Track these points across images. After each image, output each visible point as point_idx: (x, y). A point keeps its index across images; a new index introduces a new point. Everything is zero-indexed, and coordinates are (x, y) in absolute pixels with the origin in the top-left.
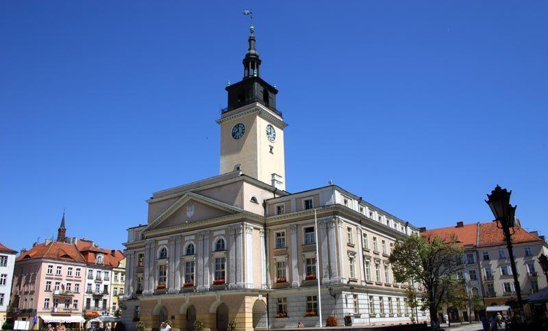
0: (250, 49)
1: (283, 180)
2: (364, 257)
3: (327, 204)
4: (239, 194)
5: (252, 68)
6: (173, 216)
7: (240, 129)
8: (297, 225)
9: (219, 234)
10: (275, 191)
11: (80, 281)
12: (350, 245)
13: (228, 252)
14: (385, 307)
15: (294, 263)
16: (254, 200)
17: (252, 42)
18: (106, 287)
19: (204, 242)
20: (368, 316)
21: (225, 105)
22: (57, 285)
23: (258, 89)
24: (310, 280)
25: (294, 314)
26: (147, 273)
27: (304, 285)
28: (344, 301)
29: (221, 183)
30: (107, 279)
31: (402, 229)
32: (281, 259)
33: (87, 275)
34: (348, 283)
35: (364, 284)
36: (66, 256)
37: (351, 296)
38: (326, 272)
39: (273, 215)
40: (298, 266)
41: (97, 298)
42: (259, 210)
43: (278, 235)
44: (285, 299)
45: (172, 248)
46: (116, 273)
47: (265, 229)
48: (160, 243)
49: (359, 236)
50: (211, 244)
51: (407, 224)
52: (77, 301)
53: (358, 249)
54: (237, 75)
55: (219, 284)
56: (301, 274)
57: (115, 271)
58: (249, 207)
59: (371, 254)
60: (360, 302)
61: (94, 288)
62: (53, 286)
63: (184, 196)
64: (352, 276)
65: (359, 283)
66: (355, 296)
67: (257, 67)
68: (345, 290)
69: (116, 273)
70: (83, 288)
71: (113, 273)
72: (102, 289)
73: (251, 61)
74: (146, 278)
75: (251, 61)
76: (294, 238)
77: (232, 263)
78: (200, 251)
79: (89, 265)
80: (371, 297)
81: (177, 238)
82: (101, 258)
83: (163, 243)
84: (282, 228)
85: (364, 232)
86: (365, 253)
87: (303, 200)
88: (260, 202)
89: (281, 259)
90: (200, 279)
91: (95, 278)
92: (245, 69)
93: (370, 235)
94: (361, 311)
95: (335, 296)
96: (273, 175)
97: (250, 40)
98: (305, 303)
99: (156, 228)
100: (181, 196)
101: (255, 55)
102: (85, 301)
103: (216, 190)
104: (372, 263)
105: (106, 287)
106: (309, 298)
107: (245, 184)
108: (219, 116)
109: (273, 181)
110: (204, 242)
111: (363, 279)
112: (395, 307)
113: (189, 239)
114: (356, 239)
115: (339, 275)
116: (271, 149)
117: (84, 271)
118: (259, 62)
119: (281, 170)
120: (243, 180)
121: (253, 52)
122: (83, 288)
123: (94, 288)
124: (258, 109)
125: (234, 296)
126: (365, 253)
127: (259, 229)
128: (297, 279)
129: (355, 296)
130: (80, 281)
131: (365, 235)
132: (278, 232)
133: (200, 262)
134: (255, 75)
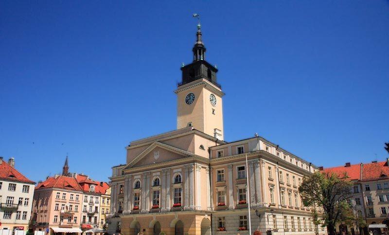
0: (197, 41)
1: (221, 133)
2: (280, 188)
3: (254, 150)
4: (191, 143)
5: (199, 54)
6: (145, 158)
7: (191, 97)
8: (232, 165)
9: (177, 171)
10: (217, 141)
11: (79, 204)
12: (270, 179)
13: (183, 183)
14: (295, 224)
15: (231, 192)
16: (202, 147)
17: (199, 35)
18: (96, 208)
19: (166, 177)
20: (283, 230)
21: (180, 80)
22: (63, 206)
23: (204, 69)
24: (242, 204)
25: (230, 228)
26: (126, 198)
27: (237, 208)
28: (266, 219)
29: (179, 135)
30: (97, 203)
31: (307, 168)
32: (221, 189)
33: (84, 199)
34: (269, 206)
35: (280, 207)
36: (69, 186)
37: (271, 216)
38: (253, 199)
39: (216, 158)
40: (233, 194)
41: (90, 216)
42: (205, 154)
43: (219, 172)
44: (224, 218)
45: (144, 181)
46: (104, 198)
47: (210, 168)
48: (135, 177)
49: (277, 173)
50: (151, 181)
51: (310, 164)
52: (76, 218)
53: (276, 182)
54: (188, 59)
55: (177, 206)
56: (235, 200)
57: (103, 197)
58: (198, 152)
59: (285, 186)
60: (278, 220)
61: (88, 209)
62: (60, 206)
63: (153, 144)
64: (272, 202)
65: (276, 207)
66: (274, 216)
67: (203, 53)
68: (267, 212)
69: (104, 198)
70: (81, 208)
71: (102, 198)
72: (94, 209)
73: (198, 49)
74: (125, 202)
75: (198, 49)
76: (230, 173)
77: (187, 192)
78: (164, 184)
79: (85, 192)
80: (285, 217)
81: (147, 174)
82: (93, 188)
83: (137, 178)
84: (221, 168)
85: (280, 170)
86: (281, 185)
87: (237, 147)
88: (206, 148)
89: (221, 189)
90: (164, 203)
91: (89, 202)
92: (194, 55)
93: (284, 173)
94: (278, 227)
95: (259, 216)
96: (215, 129)
97: (198, 35)
98: (238, 221)
99: (132, 167)
100: (151, 144)
101: (201, 45)
102: (82, 217)
103: (175, 140)
104: (286, 192)
105: (96, 208)
106: (241, 217)
107: (195, 136)
108: (176, 88)
109: (215, 134)
110: (166, 177)
111: (280, 204)
112: (302, 224)
113: (156, 175)
114: (275, 176)
115: (263, 201)
116: (213, 111)
117: (82, 196)
118: (204, 50)
119: (220, 125)
120: (194, 133)
121: (200, 42)
122: (81, 208)
123: (88, 209)
124: (204, 83)
125: (188, 215)
126: (281, 185)
127: (205, 168)
128: (232, 203)
129: (274, 216)
130: (79, 204)
131: (281, 172)
132: (219, 170)
133: (164, 191)
134: (202, 59)
